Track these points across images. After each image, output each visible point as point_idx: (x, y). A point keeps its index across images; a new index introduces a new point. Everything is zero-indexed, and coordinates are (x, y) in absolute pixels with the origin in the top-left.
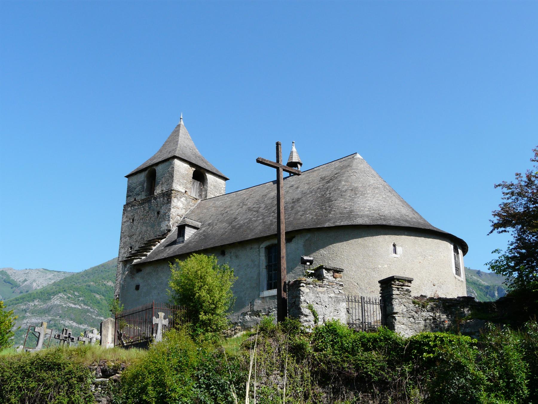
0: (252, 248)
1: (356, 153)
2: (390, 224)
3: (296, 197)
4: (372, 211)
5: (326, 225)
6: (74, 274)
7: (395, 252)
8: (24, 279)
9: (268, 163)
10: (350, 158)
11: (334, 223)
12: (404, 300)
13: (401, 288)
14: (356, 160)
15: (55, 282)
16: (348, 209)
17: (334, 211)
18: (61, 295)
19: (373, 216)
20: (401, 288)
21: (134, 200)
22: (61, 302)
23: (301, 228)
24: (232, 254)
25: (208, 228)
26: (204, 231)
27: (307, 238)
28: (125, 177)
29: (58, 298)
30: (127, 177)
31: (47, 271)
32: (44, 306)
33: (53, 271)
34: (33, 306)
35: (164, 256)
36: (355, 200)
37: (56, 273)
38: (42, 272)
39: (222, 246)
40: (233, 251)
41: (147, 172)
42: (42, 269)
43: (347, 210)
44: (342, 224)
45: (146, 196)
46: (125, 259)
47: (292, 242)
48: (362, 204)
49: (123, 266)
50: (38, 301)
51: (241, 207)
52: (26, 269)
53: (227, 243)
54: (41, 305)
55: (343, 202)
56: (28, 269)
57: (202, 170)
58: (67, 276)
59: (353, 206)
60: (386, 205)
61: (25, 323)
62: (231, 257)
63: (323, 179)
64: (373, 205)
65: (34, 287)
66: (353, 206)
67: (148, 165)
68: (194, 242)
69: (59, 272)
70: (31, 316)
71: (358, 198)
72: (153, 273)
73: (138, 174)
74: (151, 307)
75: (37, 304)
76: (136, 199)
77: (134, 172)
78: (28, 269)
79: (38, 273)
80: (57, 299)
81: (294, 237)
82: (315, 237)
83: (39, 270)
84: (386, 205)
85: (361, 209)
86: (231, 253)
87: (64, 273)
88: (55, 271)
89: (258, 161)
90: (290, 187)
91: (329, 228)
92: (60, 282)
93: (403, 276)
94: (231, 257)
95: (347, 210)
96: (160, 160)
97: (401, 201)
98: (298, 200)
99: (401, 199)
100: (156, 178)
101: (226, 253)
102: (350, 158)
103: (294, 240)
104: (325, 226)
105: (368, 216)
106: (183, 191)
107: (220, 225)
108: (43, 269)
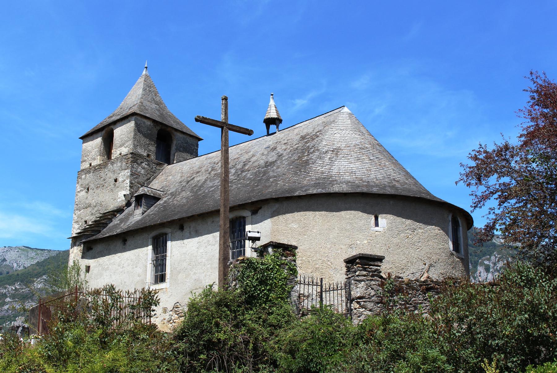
0: (213, 221)
1: (344, 106)
2: (372, 192)
3: (271, 160)
4: (353, 176)
5: (297, 194)
6: (60, 253)
7: (377, 225)
8: (3, 258)
9: (210, 121)
10: (337, 113)
11: (306, 190)
12: (373, 283)
13: (368, 268)
14: (342, 115)
15: (38, 262)
16: (326, 174)
17: (310, 176)
18: (45, 278)
19: (354, 182)
20: (368, 268)
21: (89, 165)
22: (45, 285)
23: (268, 197)
24: (192, 229)
25: (170, 199)
26: (165, 202)
27: (275, 209)
28: (202, 140)
29: (42, 280)
30: (81, 138)
31: (29, 249)
32: (26, 290)
33: (36, 249)
34: (14, 290)
35: (117, 231)
36: (335, 163)
37: (39, 252)
38: (23, 250)
39: (180, 220)
40: (193, 225)
41: (104, 132)
42: (23, 247)
43: (324, 175)
44: (315, 192)
45: (484, 158)
46: (75, 235)
47: (258, 214)
48: (342, 168)
49: (73, 244)
50: (20, 284)
51: (209, 173)
52: (5, 247)
53: (184, 215)
54: (22, 289)
55: (321, 166)
56: (7, 246)
57: (169, 129)
58: (54, 254)
59: (332, 170)
60: (372, 169)
61: (6, 310)
62: (190, 233)
63: (303, 138)
64: (356, 169)
65: (14, 267)
66: (332, 170)
67: (105, 124)
68: (152, 214)
69: (42, 250)
70: (11, 302)
71: (339, 161)
72: (105, 252)
73: (94, 135)
74: (332, 292)
75: (18, 287)
76: (92, 165)
77: (89, 133)
78: (7, 246)
79: (18, 251)
80: (42, 282)
81: (260, 208)
82: (284, 207)
83: (20, 249)
84: (372, 169)
85: (341, 174)
86: (190, 227)
87: (49, 251)
88: (39, 249)
89: (197, 120)
90: (266, 148)
91: (300, 197)
92: (43, 262)
93: (370, 253)
94: (190, 233)
95: (324, 175)
96: (118, 117)
97: (393, 163)
98: (273, 163)
99: (394, 161)
100: (114, 139)
101: (185, 227)
102: (337, 113)
103: (260, 211)
104: (295, 195)
105: (348, 182)
106: (145, 154)
107: (184, 194)
108: (25, 247)
